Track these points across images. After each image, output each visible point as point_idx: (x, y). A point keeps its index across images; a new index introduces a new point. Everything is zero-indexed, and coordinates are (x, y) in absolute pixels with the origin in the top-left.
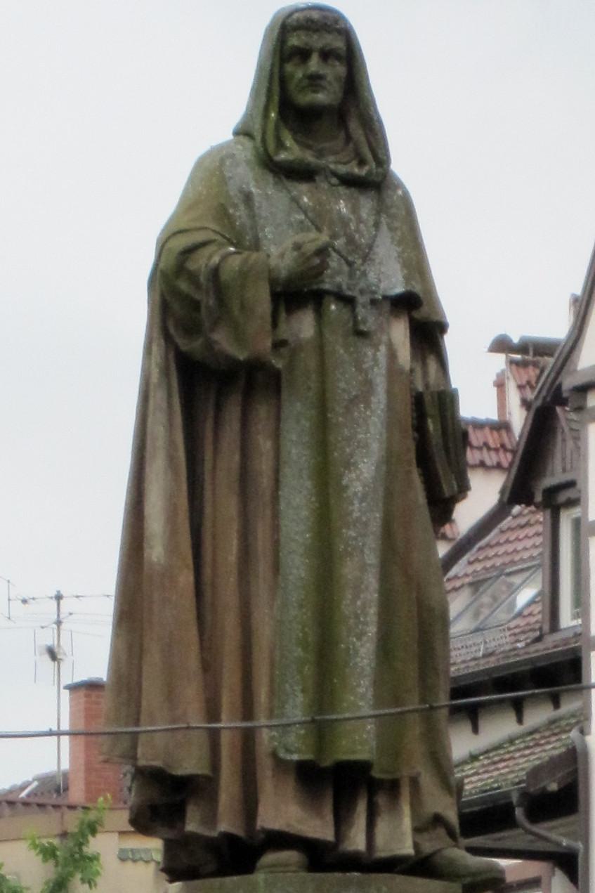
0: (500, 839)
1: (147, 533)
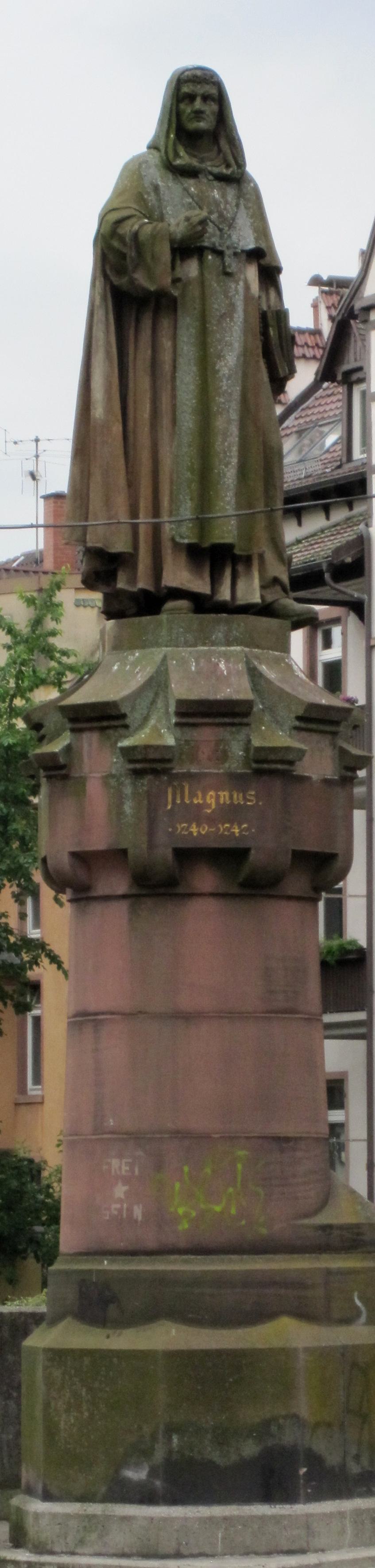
0: (315, 593)
1: (93, 400)
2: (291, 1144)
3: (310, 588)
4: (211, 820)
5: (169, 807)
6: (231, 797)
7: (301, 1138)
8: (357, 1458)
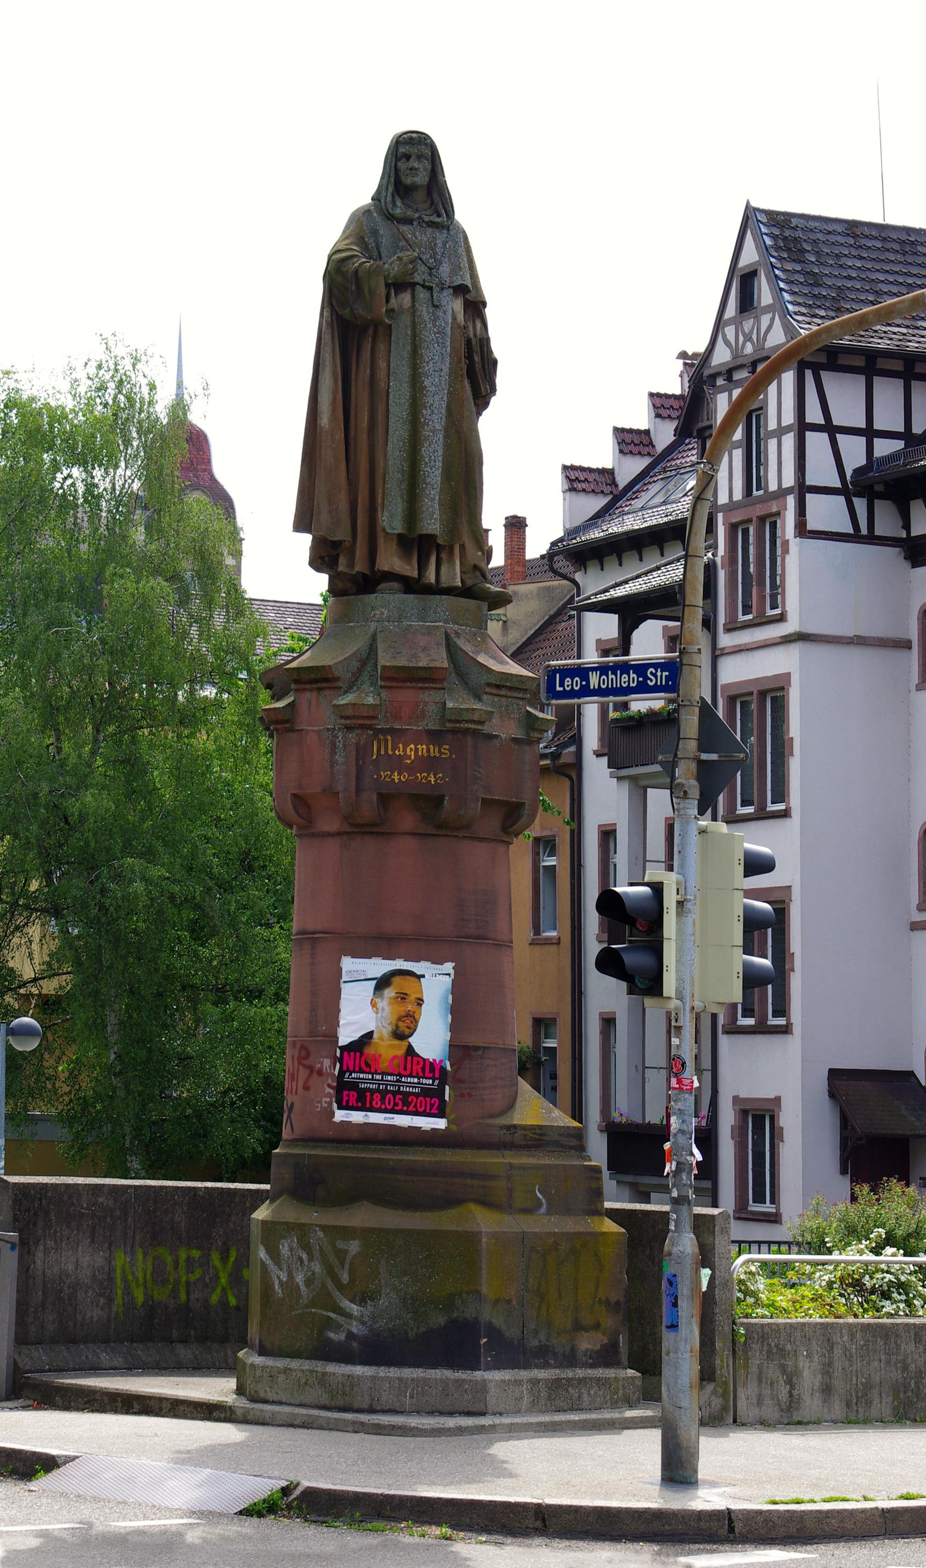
0: (674, 611)
1: (319, 410)
2: (480, 1053)
3: (668, 607)
4: (411, 769)
5: (374, 757)
6: (428, 750)
7: (489, 1048)
8: (536, 1332)
